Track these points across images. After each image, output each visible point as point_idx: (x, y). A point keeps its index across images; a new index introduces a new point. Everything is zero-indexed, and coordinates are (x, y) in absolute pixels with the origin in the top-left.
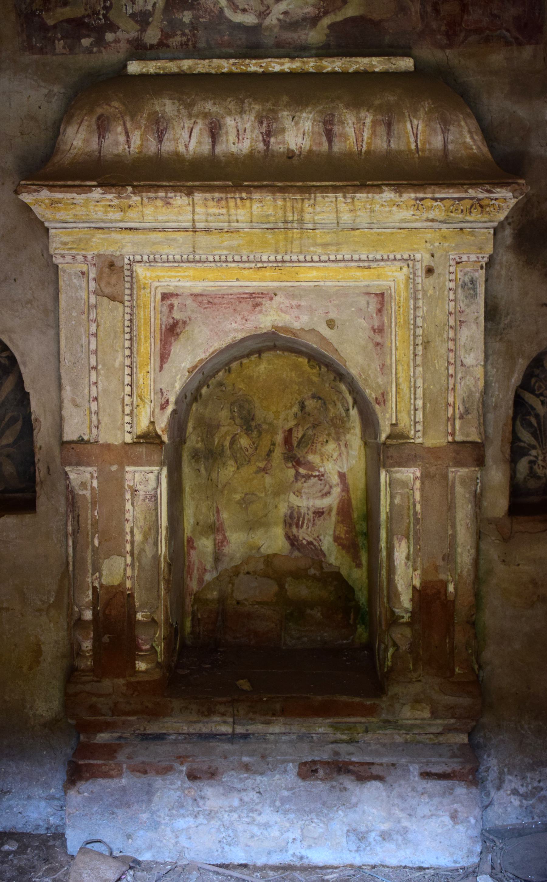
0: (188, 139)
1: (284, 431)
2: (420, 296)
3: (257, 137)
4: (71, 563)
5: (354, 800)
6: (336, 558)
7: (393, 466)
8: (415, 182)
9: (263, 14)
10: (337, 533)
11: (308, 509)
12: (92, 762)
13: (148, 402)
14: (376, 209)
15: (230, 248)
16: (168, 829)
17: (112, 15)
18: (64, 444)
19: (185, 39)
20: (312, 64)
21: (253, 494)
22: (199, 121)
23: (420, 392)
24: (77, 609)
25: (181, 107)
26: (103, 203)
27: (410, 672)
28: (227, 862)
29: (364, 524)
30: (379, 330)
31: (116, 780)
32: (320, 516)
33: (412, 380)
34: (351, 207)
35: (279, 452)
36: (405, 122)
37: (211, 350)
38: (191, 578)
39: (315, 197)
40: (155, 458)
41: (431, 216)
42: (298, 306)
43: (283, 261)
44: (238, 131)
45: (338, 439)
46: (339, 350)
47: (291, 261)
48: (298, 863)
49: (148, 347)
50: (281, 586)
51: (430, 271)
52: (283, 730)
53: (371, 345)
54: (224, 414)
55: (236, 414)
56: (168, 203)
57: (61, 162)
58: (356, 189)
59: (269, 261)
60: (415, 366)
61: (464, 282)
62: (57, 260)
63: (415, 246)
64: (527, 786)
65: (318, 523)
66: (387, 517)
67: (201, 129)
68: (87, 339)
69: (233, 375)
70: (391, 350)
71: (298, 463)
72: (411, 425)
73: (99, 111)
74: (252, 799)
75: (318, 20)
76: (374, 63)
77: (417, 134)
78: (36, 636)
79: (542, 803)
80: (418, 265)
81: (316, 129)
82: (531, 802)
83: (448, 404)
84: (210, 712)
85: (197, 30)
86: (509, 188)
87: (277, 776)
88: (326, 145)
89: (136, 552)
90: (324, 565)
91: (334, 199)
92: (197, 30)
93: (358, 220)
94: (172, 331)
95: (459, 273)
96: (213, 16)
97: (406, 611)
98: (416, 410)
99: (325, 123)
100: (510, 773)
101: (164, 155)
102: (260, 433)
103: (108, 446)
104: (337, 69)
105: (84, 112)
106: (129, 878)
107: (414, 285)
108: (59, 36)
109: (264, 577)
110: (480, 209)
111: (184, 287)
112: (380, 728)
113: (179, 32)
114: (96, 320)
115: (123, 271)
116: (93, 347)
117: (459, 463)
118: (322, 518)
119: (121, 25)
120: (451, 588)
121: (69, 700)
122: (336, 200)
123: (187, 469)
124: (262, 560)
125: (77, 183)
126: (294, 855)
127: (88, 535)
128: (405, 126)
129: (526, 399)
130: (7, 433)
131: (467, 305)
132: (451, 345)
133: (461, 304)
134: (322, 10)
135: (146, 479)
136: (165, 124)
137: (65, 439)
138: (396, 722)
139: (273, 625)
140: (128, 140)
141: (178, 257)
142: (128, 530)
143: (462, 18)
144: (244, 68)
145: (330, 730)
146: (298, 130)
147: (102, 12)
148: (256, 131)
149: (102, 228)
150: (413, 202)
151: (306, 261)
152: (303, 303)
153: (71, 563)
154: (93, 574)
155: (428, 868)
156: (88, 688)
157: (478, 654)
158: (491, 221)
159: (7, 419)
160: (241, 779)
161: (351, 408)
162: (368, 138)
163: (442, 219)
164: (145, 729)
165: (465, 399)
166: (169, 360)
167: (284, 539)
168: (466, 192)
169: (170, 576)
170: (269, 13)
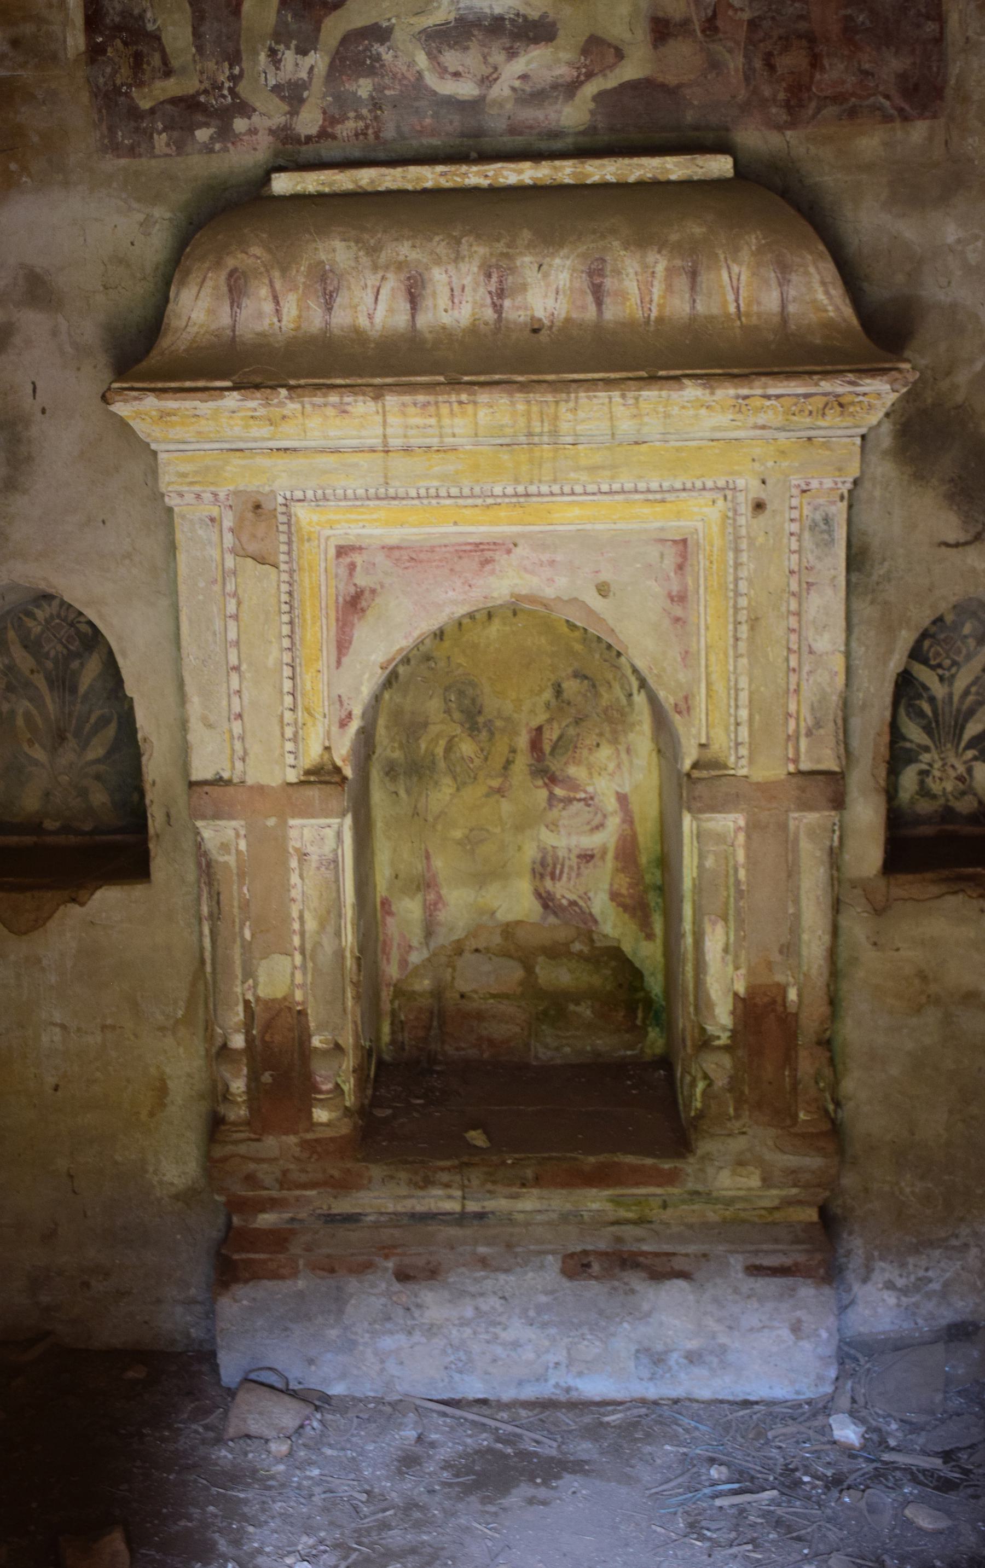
0: (371, 305)
1: (530, 732)
2: (744, 545)
3: (483, 299)
4: (208, 962)
5: (646, 1307)
6: (615, 926)
7: (701, 811)
8: (736, 371)
9: (487, 81)
10: (616, 887)
11: (570, 850)
12: (252, 1256)
14: (674, 413)
16: (369, 1351)
17: (243, 88)
18: (192, 784)
19: (361, 124)
20: (568, 171)
21: (482, 829)
22: (391, 276)
23: (744, 697)
24: (220, 1031)
25: (361, 253)
26: (240, 414)
27: (730, 1119)
28: (458, 1396)
29: (658, 873)
30: (680, 598)
31: (289, 1282)
32: (588, 862)
33: (732, 678)
34: (635, 411)
36: (719, 269)
37: (416, 634)
38: (388, 960)
39: (577, 398)
40: (334, 804)
41: (760, 422)
42: (552, 563)
43: (527, 495)
44: (452, 290)
45: (615, 741)
46: (617, 630)
47: (539, 495)
48: (563, 1398)
49: (318, 630)
50: (529, 969)
51: (759, 506)
52: (537, 1205)
53: (666, 623)
54: (434, 706)
55: (453, 705)
56: (345, 412)
57: (173, 348)
58: (642, 383)
59: (505, 495)
60: (737, 657)
61: (813, 520)
62: (171, 501)
63: (736, 468)
64: (908, 1277)
65: (585, 871)
66: (694, 885)
67: (393, 289)
68: (222, 623)
69: (447, 644)
70: (699, 628)
71: (552, 779)
72: (730, 748)
73: (231, 262)
74: (493, 1308)
75: (577, 88)
76: (668, 166)
77: (738, 289)
78: (158, 1067)
79: (930, 1300)
80: (741, 498)
81: (577, 285)
82: (913, 1300)
83: (789, 715)
84: (427, 1183)
85: (380, 108)
86: (885, 378)
87: (531, 1275)
88: (592, 308)
89: (308, 947)
90: (595, 937)
91: (607, 400)
92: (380, 108)
93: (645, 430)
94: (354, 604)
96: (406, 86)
97: (724, 1028)
98: (738, 724)
99: (591, 274)
100: (882, 1258)
102: (492, 734)
105: (207, 265)
106: (315, 1424)
107: (735, 528)
108: (160, 126)
109: (504, 955)
110: (839, 409)
111: (371, 536)
112: (684, 1202)
113: (352, 114)
114: (235, 595)
115: (275, 517)
116: (232, 635)
117: (805, 806)
118: (591, 864)
119: (257, 105)
120: (792, 995)
121: (212, 1166)
122: (610, 402)
123: (378, 796)
124: (498, 931)
125: (200, 384)
126: (557, 1385)
127: (234, 922)
129: (915, 674)
130: (95, 741)
131: (819, 558)
132: (793, 623)
133: (810, 557)
134: (584, 70)
135: (321, 835)
136: (336, 282)
137: (196, 776)
138: (709, 1194)
139: (517, 1029)
140: (277, 309)
141: (361, 492)
142: (295, 914)
143: (812, 77)
144: (458, 179)
145: (609, 1207)
146: (548, 285)
147: (227, 85)
148: (482, 290)
149: (241, 450)
150: (733, 402)
151: (563, 494)
152: (558, 559)
153: (208, 962)
154: (243, 983)
155: (757, 1403)
156: (242, 1149)
157: (835, 1086)
158: (859, 427)
159: (92, 720)
160: (475, 1279)
161: (635, 691)
162: (660, 297)
163: (779, 425)
164: (330, 1208)
165: (816, 704)
166: (351, 650)
167: (532, 898)
168: (817, 385)
169: (359, 975)
170: (496, 80)
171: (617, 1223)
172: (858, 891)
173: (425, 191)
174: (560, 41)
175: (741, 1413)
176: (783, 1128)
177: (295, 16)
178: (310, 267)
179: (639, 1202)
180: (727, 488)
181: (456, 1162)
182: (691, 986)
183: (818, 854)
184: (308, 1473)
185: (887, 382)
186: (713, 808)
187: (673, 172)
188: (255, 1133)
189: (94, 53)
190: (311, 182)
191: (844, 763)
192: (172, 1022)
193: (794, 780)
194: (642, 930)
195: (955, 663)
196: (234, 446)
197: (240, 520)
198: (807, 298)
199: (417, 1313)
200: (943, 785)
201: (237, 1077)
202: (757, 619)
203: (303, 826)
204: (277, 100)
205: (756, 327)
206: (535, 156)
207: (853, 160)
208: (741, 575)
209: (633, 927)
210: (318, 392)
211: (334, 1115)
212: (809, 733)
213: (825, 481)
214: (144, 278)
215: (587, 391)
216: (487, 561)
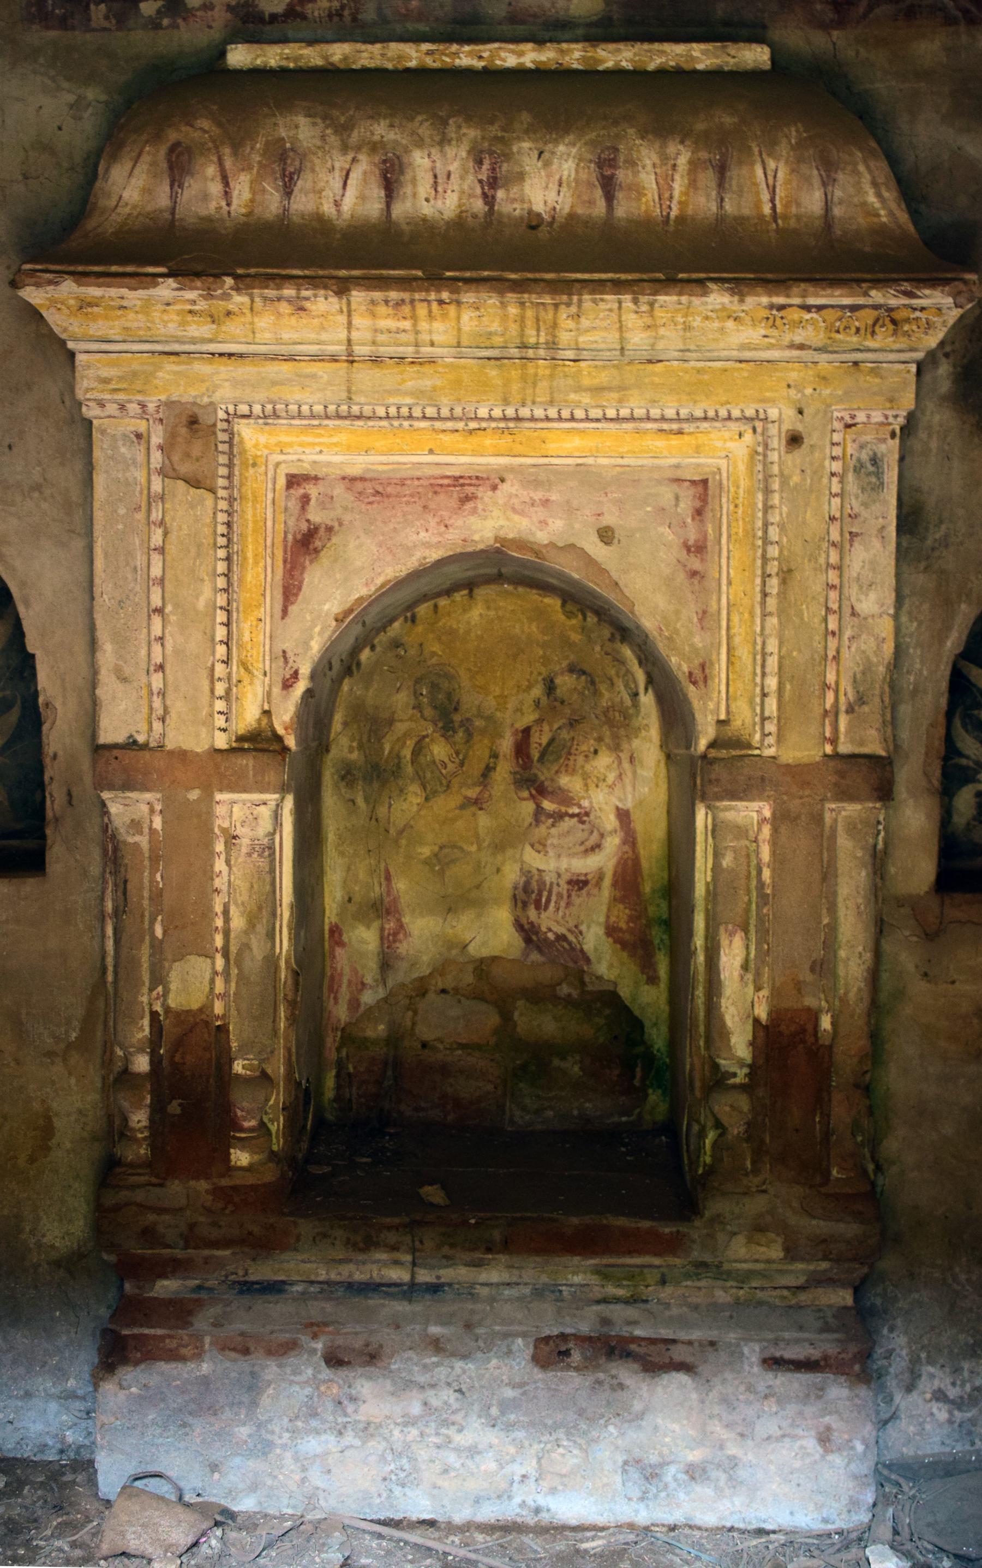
0: (340, 190)
5: (638, 1406)
6: (611, 966)
7: (719, 798)
8: (770, 276)
10: (613, 919)
11: (559, 875)
12: (147, 1331)
14: (695, 324)
15: (418, 393)
18: (98, 749)
20: (577, 55)
23: (772, 663)
25: (329, 131)
26: (178, 307)
27: (747, 1175)
28: (398, 1516)
29: (664, 905)
30: (698, 549)
31: (191, 1365)
32: (580, 889)
33: (759, 640)
34: (648, 321)
35: (504, 771)
36: (752, 164)
37: (379, 581)
39: (580, 301)
40: (271, 777)
41: (798, 339)
42: (546, 502)
43: (518, 419)
44: (435, 177)
45: (616, 748)
46: (621, 584)
47: (533, 419)
48: (531, 1520)
49: (260, 572)
50: (506, 1017)
51: (795, 440)
52: (505, 1276)
53: (681, 577)
54: (402, 699)
56: (302, 309)
57: (100, 230)
58: (658, 286)
59: (491, 418)
60: (764, 615)
61: (859, 460)
62: (91, 411)
63: (768, 394)
64: (963, 1385)
65: (576, 900)
67: (365, 173)
68: (145, 558)
69: (420, 629)
71: (541, 791)
72: (754, 724)
73: (173, 136)
74: (446, 1403)
76: (694, 54)
77: (774, 187)
78: (43, 1101)
80: (773, 430)
81: (584, 176)
82: (969, 1415)
83: (826, 686)
84: (369, 1244)
87: (494, 1362)
89: (233, 949)
90: (587, 979)
91: (616, 306)
94: (306, 544)
95: (849, 444)
97: (741, 1063)
98: (764, 695)
99: (600, 164)
100: (930, 1362)
102: (469, 735)
103: (182, 755)
104: (624, 64)
105: (145, 137)
106: (213, 1542)
107: (765, 465)
110: (891, 327)
111: (329, 464)
112: (688, 1276)
114: (162, 523)
115: (215, 433)
116: (156, 571)
117: (844, 795)
118: (584, 892)
120: (826, 1023)
121: (104, 1219)
122: (620, 308)
123: (330, 801)
124: (470, 968)
125: (130, 269)
127: (143, 916)
128: (752, 171)
129: (973, 679)
131: (865, 505)
132: (833, 577)
136: (297, 163)
139: (490, 1087)
140: (227, 191)
141: (318, 408)
142: (218, 908)
144: (448, 60)
145: (594, 1280)
146: (549, 176)
148: (471, 178)
151: (560, 419)
152: (553, 498)
155: (774, 1532)
156: (139, 1196)
157: (874, 1143)
163: (820, 344)
164: (246, 1274)
166: (300, 597)
168: (866, 294)
172: (905, 911)
175: (754, 1543)
176: (811, 1187)
178: (267, 143)
182: (702, 1014)
183: (859, 854)
185: (949, 295)
187: (701, 61)
188: (157, 1176)
192: (62, 1046)
193: (831, 764)
194: (643, 973)
196: (167, 348)
198: (856, 200)
199: (350, 1408)
205: (795, 231)
208: (771, 520)
210: (271, 284)
211: (256, 1158)
212: (850, 710)
213: (873, 414)
214: (72, 169)
215: (593, 292)
216: (467, 499)
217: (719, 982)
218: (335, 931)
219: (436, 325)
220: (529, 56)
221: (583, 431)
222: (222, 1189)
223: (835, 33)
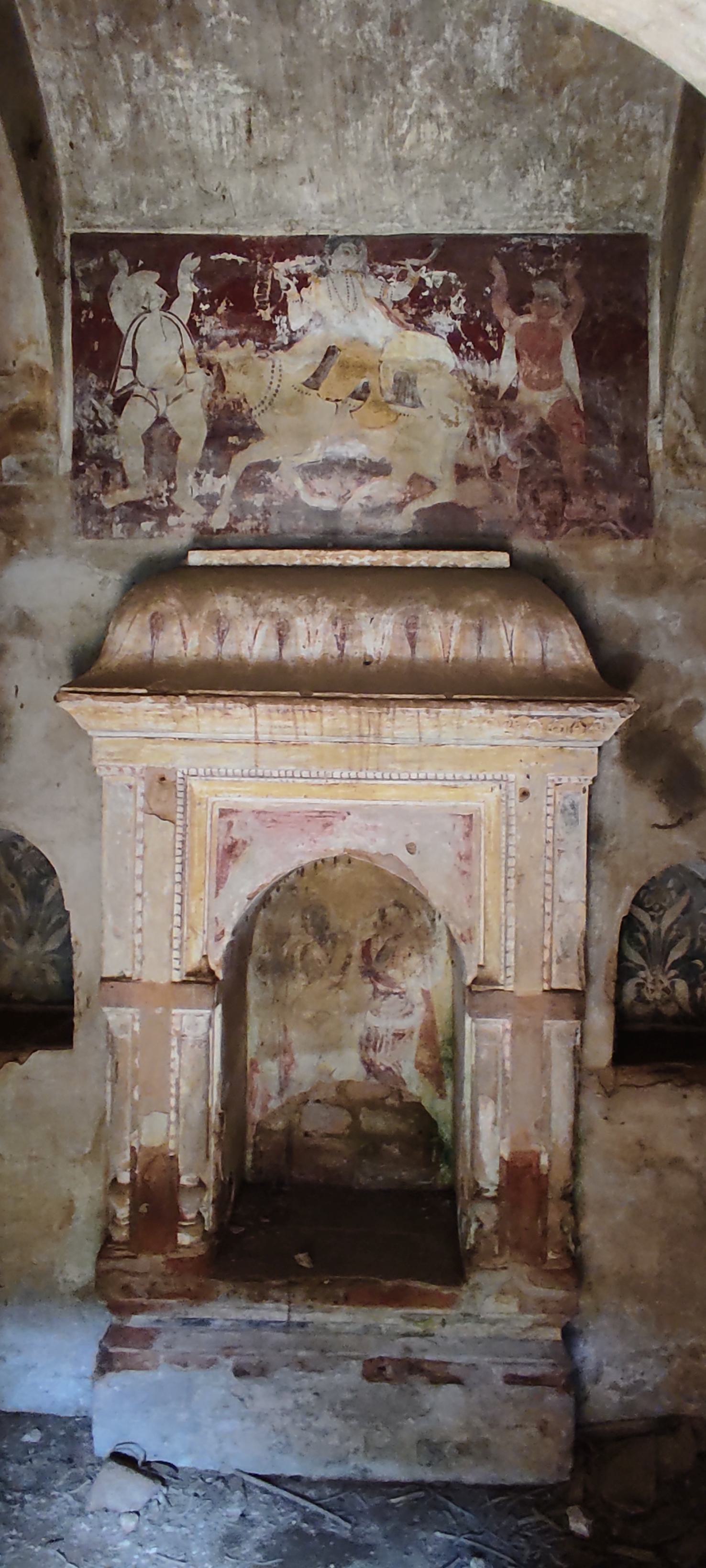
0: (251, 640)
2: (513, 821)
9: (343, 499)
10: (419, 1058)
13: (200, 933)
15: (297, 763)
17: (176, 498)
20: (395, 557)
23: (511, 932)
27: (495, 1256)
30: (467, 857)
33: (503, 917)
35: (355, 964)
37: (275, 875)
39: (394, 712)
41: (526, 735)
45: (421, 953)
49: (203, 869)
50: (355, 1116)
51: (525, 794)
54: (295, 921)
58: (442, 703)
61: (564, 806)
66: (473, 1071)
69: (305, 878)
73: (153, 608)
80: (512, 787)
83: (544, 947)
84: (262, 1297)
89: (182, 1106)
94: (231, 851)
95: (558, 796)
97: (492, 1184)
98: (506, 952)
99: (407, 626)
101: (225, 658)
102: (334, 943)
103: (152, 986)
105: (137, 609)
108: (118, 519)
111: (245, 803)
112: (459, 1321)
113: (249, 516)
116: (139, 871)
117: (555, 1016)
119: (185, 508)
120: (544, 1161)
123: (253, 984)
128: (498, 633)
132: (548, 878)
133: (561, 831)
140: (184, 640)
141: (238, 771)
143: (564, 508)
151: (383, 779)
152: (380, 824)
156: (121, 1264)
167: (359, 1062)
171: (407, 1335)
172: (594, 1078)
173: (294, 567)
174: (393, 475)
177: (214, 453)
179: (424, 1319)
180: (502, 780)
181: (285, 1281)
184: (147, 1551)
186: (489, 1014)
189: (77, 472)
190: (216, 558)
191: (584, 982)
195: (661, 908)
197: (149, 788)
200: (654, 995)
201: (123, 1206)
202: (522, 875)
203: (182, 1015)
204: (198, 505)
206: (372, 547)
207: (596, 562)
209: (431, 1088)
212: (559, 961)
217: (478, 1132)
218: (254, 1063)
219: (308, 724)
220: (366, 558)
221: (395, 786)
222: (173, 1260)
223: (548, 542)
